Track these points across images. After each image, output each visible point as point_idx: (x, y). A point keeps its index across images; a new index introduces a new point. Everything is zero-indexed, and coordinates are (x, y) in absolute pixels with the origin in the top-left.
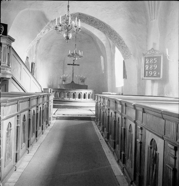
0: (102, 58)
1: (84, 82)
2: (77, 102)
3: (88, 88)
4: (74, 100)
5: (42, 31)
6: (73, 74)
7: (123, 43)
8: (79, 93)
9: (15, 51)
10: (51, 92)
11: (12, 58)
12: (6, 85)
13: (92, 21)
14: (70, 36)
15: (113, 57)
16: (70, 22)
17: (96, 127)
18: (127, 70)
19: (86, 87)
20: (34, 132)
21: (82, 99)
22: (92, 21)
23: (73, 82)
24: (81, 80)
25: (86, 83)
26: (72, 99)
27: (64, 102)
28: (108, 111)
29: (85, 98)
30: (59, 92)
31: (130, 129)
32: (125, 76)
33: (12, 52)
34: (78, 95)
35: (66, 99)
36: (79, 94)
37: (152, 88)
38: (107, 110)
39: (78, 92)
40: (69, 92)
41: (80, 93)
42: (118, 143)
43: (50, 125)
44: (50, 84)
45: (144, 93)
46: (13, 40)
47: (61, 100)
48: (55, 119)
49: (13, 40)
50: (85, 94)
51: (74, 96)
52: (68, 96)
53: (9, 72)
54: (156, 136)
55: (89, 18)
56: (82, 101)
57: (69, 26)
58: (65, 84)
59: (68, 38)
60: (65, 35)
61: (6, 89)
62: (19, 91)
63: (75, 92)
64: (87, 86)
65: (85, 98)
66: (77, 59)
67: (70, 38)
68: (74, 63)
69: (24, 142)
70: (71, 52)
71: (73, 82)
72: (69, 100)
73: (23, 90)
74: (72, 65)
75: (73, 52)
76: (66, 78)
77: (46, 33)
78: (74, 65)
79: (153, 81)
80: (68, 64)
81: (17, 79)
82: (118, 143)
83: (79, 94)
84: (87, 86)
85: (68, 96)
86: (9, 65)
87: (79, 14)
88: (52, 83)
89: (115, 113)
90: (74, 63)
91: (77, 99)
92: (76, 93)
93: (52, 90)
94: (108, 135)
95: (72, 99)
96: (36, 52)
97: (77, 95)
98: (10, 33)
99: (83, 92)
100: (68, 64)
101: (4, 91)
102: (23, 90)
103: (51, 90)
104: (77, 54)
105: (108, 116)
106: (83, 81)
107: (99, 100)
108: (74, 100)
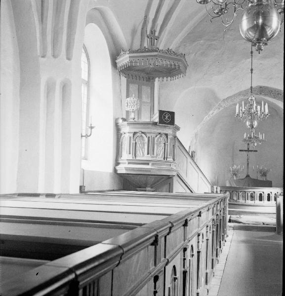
1: (265, 176)
2: (257, 206)
3: (273, 185)
5: (211, 112)
6: (248, 164)
8: (260, 193)
9: (183, 144)
10: (217, 192)
11: (177, 150)
12: (170, 184)
13: (278, 94)
14: (256, 124)
16: (254, 107)
19: (269, 184)
21: (265, 202)
22: (278, 94)
23: (248, 176)
24: (261, 173)
25: (269, 178)
26: (249, 202)
27: (239, 207)
29: (269, 199)
30: (229, 191)
33: (177, 144)
34: (258, 195)
35: (241, 201)
36: (261, 195)
39: (258, 191)
40: (245, 192)
41: (262, 193)
43: (229, 236)
44: (214, 180)
46: (178, 129)
47: (233, 203)
48: (232, 228)
49: (178, 129)
50: (269, 194)
51: (261, 198)
52: (245, 198)
53: (175, 168)
54: (157, 6)
55: (274, 91)
56: (265, 205)
58: (237, 180)
59: (252, 127)
60: (248, 123)
61: (170, 190)
62: (184, 191)
63: (254, 192)
64: (271, 182)
65: (269, 199)
66: (256, 144)
67: (255, 127)
68: (248, 149)
70: (247, 136)
71: (248, 176)
72: (244, 204)
73: (190, 189)
75: (250, 135)
76: (238, 171)
77: (214, 114)
78: (248, 150)
80: (240, 151)
84: (271, 182)
86: (174, 159)
87: (261, 87)
88: (217, 178)
90: (248, 149)
91: (257, 202)
92: (256, 193)
93: (219, 189)
96: (196, 137)
98: (177, 122)
99: (266, 191)
100: (240, 151)
101: (168, 190)
102: (190, 189)
103: (217, 189)
104: (256, 138)
106: (264, 174)
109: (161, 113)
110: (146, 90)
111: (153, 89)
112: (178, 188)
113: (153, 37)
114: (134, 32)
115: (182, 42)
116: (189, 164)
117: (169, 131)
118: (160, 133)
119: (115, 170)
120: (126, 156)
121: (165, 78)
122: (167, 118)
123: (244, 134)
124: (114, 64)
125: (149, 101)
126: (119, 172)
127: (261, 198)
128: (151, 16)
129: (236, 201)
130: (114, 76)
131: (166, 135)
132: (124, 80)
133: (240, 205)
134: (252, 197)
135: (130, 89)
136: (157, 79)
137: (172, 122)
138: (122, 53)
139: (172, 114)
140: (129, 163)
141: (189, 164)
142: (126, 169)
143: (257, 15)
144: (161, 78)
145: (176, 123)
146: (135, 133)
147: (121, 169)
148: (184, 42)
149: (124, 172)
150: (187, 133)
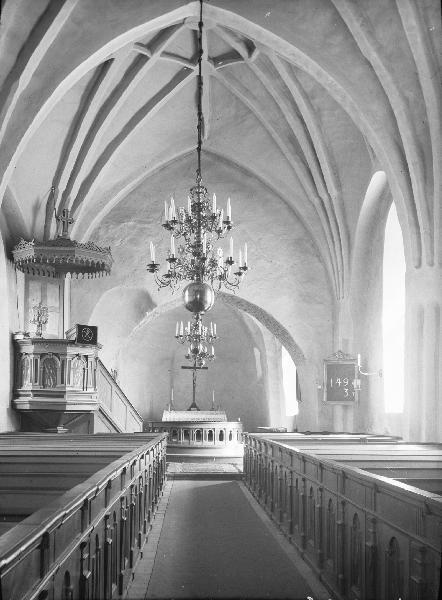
0: (257, 352)
2: (205, 448)
4: (199, 444)
7: (290, 338)
11: (99, 375)
15: (277, 364)
17: (244, 489)
18: (302, 386)
20: (113, 581)
26: (196, 443)
28: (340, 506)
29: (221, 438)
31: (354, 523)
32: (299, 397)
33: (99, 367)
34: (208, 433)
37: (344, 419)
38: (334, 503)
42: (354, 582)
45: (332, 427)
57: (204, 259)
69: (62, 397)
74: (190, 368)
78: (194, 368)
79: (345, 407)
80: (183, 367)
81: (107, 410)
82: (354, 582)
83: (211, 432)
85: (187, 435)
89: (304, 480)
91: (217, 442)
94: (281, 513)
95: (196, 443)
97: (217, 434)
100: (183, 367)
105: (304, 497)
107: (263, 451)
108: (199, 444)
109: (80, 328)
110: (52, 290)
111: (61, 288)
112: (100, 427)
113: (65, 219)
114: (36, 209)
115: (102, 223)
116: (114, 395)
117: (89, 351)
118: (77, 355)
119: (13, 405)
120: (28, 386)
121: (81, 274)
122: (87, 336)
123: (226, 201)
124: (10, 256)
125: (57, 305)
126: (19, 407)
127: (211, 436)
128: (62, 187)
129: (176, 443)
130: (9, 273)
131: (86, 357)
132: (21, 275)
133: (181, 448)
134: (211, 436)
135: (30, 288)
136: (69, 274)
137: (93, 341)
138: (23, 242)
139: (94, 329)
140: (35, 396)
141: (114, 395)
142: (30, 403)
143: (197, 292)
144: (81, 274)
145: (98, 341)
146: (42, 355)
147: (24, 403)
148: (106, 221)
149: (27, 407)
150: (109, 351)
